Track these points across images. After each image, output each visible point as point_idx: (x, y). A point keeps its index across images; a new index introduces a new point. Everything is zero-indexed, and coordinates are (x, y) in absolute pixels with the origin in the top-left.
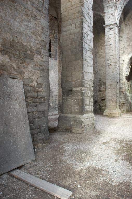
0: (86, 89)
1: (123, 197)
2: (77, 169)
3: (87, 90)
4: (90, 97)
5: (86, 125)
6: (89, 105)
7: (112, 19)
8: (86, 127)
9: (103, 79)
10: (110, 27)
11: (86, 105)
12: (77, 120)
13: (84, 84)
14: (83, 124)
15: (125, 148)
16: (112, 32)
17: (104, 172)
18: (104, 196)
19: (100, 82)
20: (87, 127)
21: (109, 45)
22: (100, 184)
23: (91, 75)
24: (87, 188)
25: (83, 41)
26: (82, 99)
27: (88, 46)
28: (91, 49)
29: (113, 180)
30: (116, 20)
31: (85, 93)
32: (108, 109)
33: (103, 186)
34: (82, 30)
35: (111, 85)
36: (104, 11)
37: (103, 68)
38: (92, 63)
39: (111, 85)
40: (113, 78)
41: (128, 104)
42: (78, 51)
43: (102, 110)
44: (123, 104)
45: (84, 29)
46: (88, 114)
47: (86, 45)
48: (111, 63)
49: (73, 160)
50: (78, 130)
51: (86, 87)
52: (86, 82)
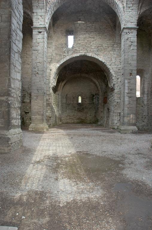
0: (13, 99)
1: (74, 215)
2: (15, 198)
3: (14, 100)
4: (17, 109)
5: (13, 142)
6: (16, 119)
7: (41, 22)
8: (13, 144)
9: (28, 89)
10: (38, 30)
11: (13, 118)
12: (2, 137)
13: (11, 93)
14: (10, 141)
15: (62, 164)
16: (41, 37)
17: (48, 195)
18: (56, 220)
19: (24, 92)
20: (14, 145)
21: (37, 50)
22: (47, 209)
23: (19, 83)
24: (33, 217)
25: (11, 40)
26: (7, 111)
27: (16, 47)
28: (19, 52)
29: (59, 201)
30: (46, 24)
31: (11, 104)
32: (34, 123)
33: (51, 209)
34: (10, 25)
35: (37, 96)
36: (33, 10)
37: (27, 75)
38: (20, 68)
39: (37, 96)
40: (40, 89)
41: (54, 118)
42: (4, 51)
43: (25, 125)
44: (49, 118)
45: (12, 25)
46: (15, 130)
47: (14, 45)
48: (39, 71)
49: (6, 187)
50: (4, 150)
51: (12, 97)
52: (13, 91)
